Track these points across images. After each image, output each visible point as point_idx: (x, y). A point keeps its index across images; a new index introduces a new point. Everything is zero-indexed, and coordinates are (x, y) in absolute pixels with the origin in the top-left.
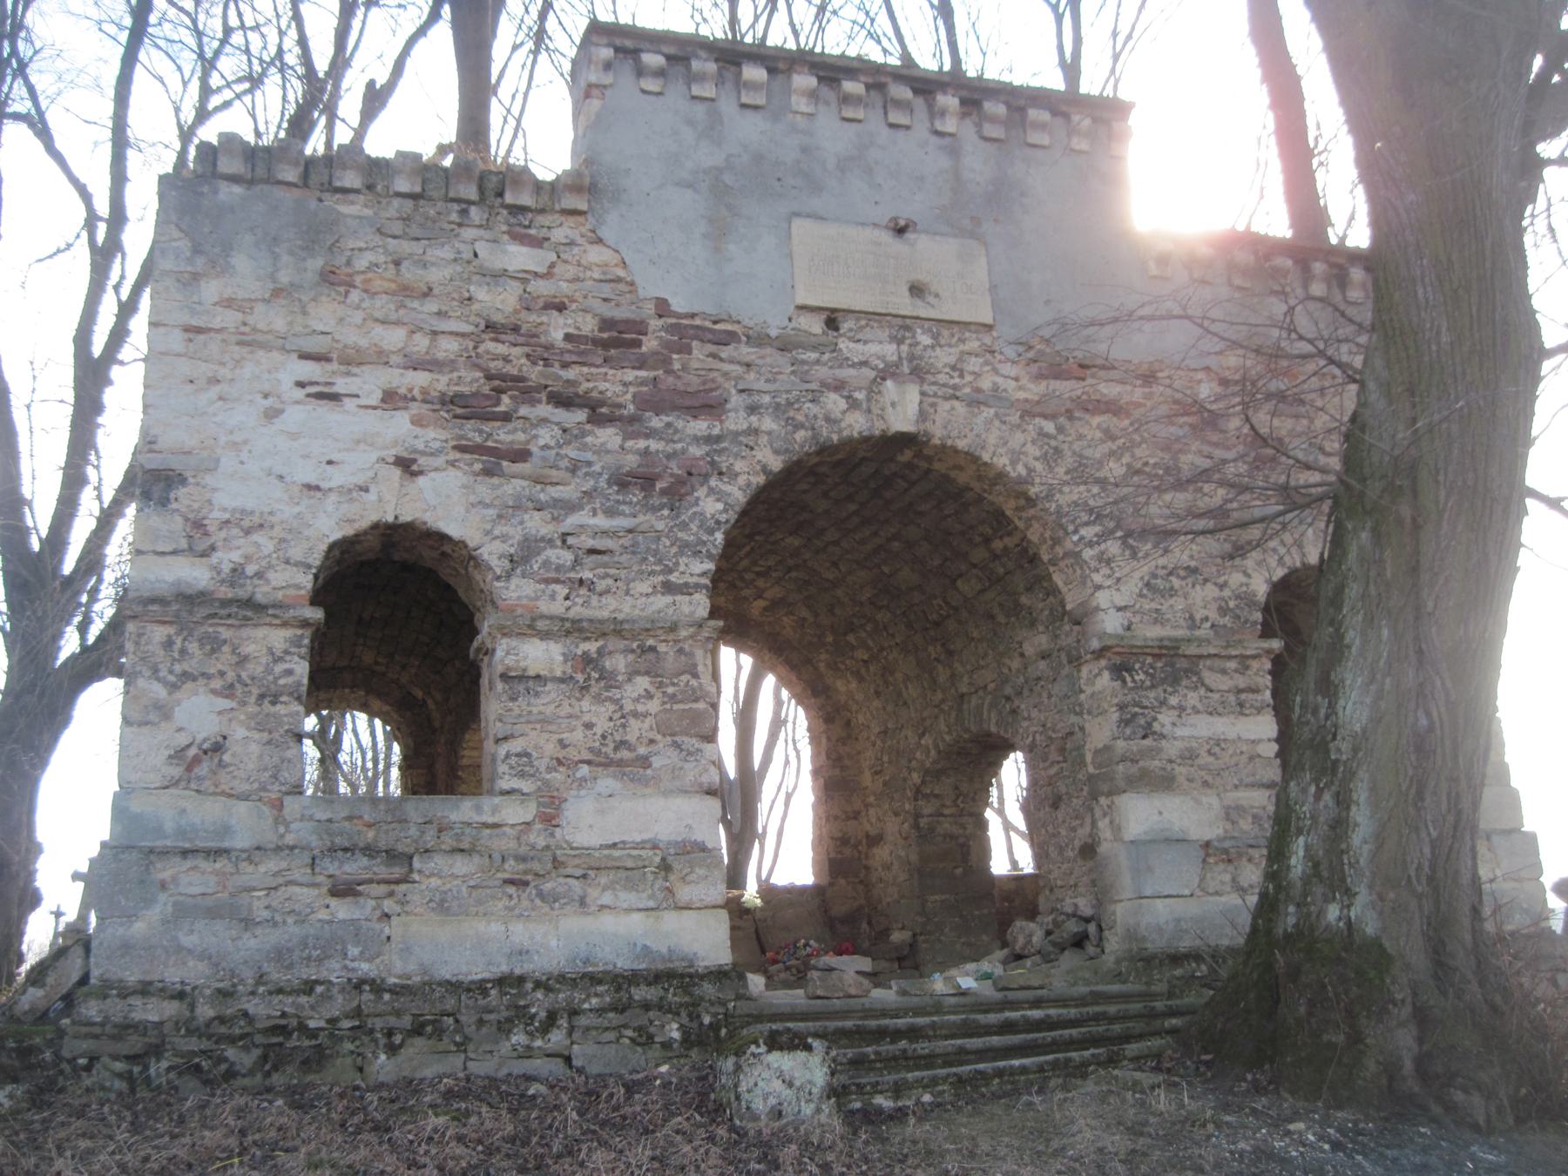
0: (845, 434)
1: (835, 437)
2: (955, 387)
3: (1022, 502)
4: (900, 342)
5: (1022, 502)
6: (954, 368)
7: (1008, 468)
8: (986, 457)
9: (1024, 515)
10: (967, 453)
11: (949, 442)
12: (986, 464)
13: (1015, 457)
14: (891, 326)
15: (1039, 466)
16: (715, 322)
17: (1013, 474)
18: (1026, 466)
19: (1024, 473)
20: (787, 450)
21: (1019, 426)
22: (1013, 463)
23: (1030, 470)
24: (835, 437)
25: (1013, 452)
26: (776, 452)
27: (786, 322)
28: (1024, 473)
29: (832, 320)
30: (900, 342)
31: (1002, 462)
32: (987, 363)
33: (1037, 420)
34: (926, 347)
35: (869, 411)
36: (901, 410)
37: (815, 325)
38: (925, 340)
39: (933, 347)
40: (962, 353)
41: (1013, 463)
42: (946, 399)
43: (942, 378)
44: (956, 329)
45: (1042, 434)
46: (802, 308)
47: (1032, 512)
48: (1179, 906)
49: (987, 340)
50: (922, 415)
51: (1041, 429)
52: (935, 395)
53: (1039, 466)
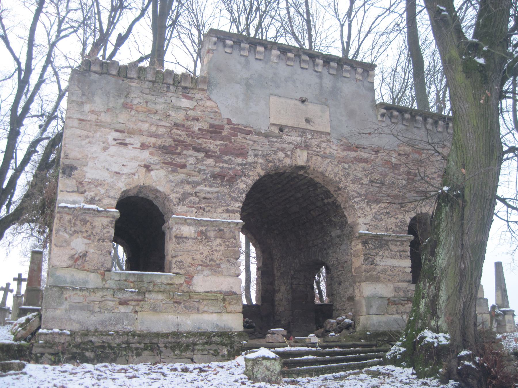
2: (318, 152)
3: (336, 189)
8: (327, 174)
9: (337, 193)
12: (326, 177)
19: (338, 180)
22: (335, 177)
28: (338, 180)
32: (328, 145)
34: (310, 139)
35: (292, 158)
36: (301, 158)
37: (276, 130)
41: (335, 177)
47: (339, 192)
49: (328, 138)
50: (308, 160)
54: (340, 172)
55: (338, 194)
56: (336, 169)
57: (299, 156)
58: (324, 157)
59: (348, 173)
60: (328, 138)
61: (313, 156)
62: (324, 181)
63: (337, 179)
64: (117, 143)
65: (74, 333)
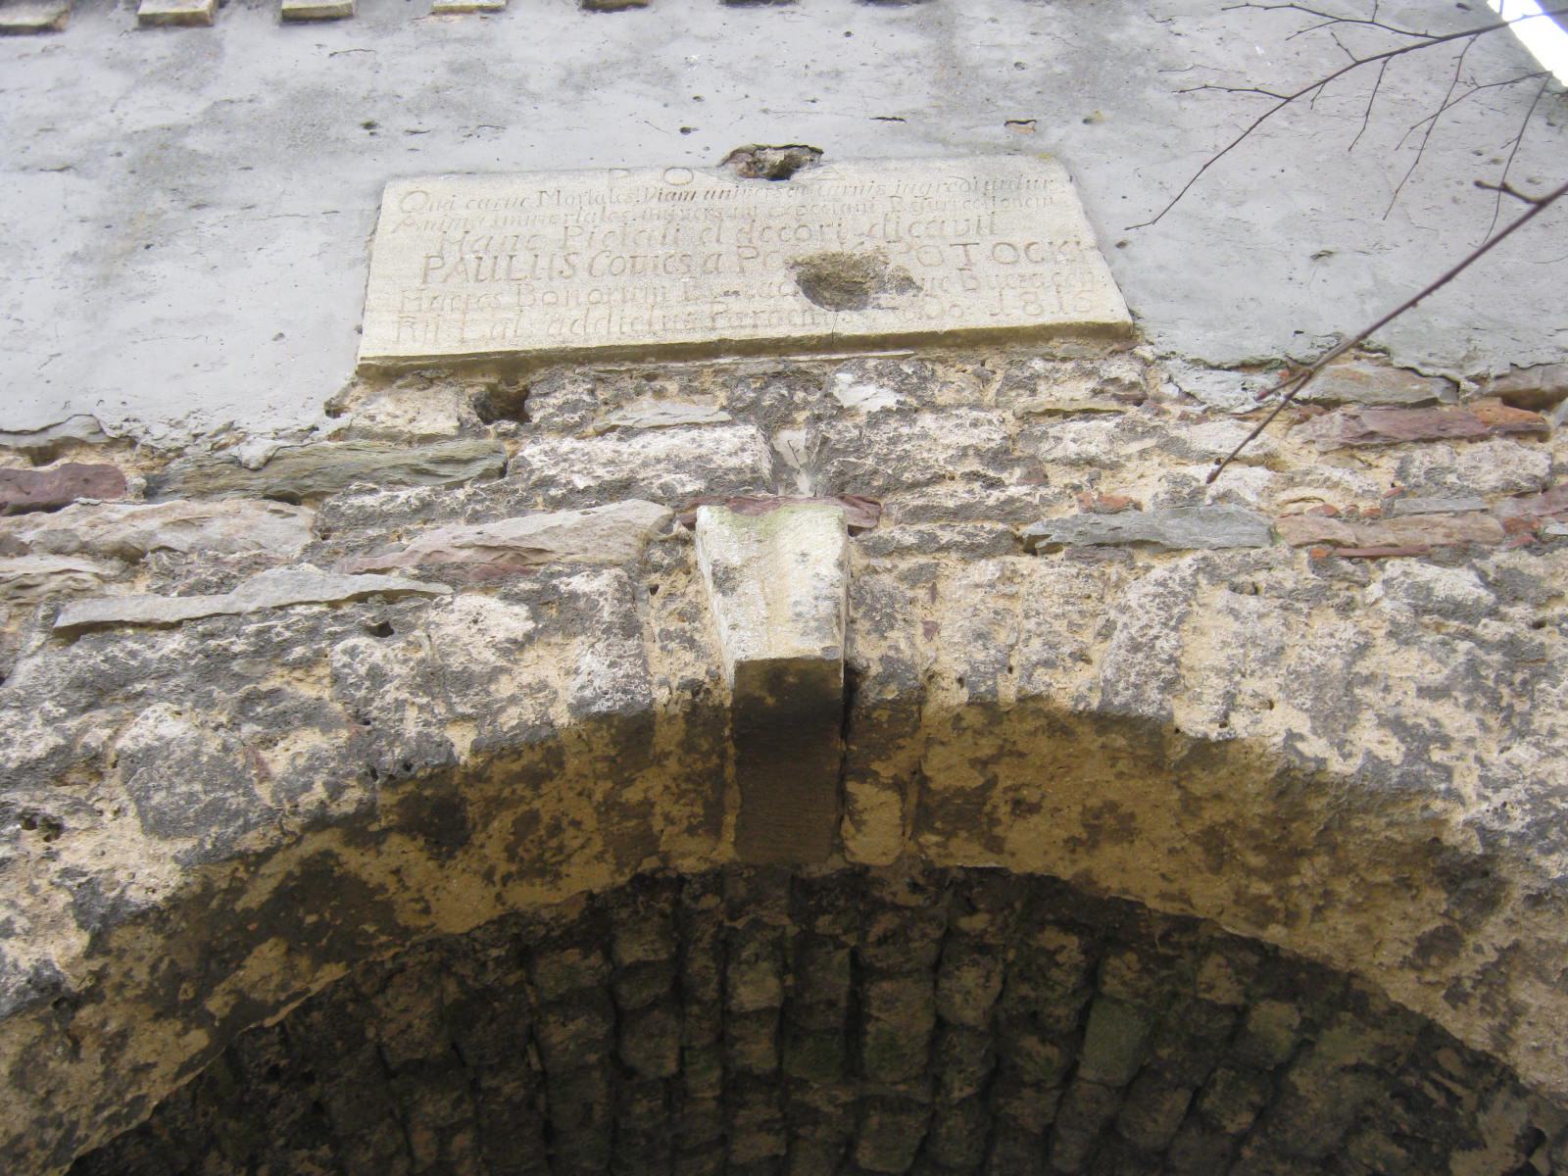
0: (509, 719)
1: (462, 740)
2: (1010, 511)
3: (1432, 907)
4: (773, 421)
5: (1432, 907)
6: (1000, 457)
7: (1315, 747)
8: (1195, 719)
9: (1466, 966)
10: (1103, 720)
11: (1008, 690)
12: (1205, 752)
13: (1336, 702)
14: (730, 380)
15: (1454, 717)
16: (42, 456)
17: (1337, 766)
18: (1396, 725)
19: (1392, 750)
20: (214, 811)
21: (1316, 597)
22: (1335, 719)
23: (1419, 739)
24: (462, 740)
25: (1320, 680)
26: (159, 826)
27: (315, 415)
28: (1392, 750)
29: (505, 389)
30: (773, 421)
31: (1277, 724)
32: (1131, 431)
33: (1394, 568)
34: (876, 420)
35: (630, 627)
36: (777, 593)
37: (438, 413)
38: (876, 397)
39: (905, 413)
40: (1026, 416)
41: (1335, 719)
42: (973, 551)
43: (952, 494)
44: (994, 360)
45: (1426, 605)
46: (385, 374)
47: (1493, 934)
48: (534, 378)
49: (1123, 370)
50: (858, 602)
51: (1426, 590)
52: (927, 544)
53: (1454, 717)
54: (1386, 657)
55: (1493, 978)
56: (1324, 638)
57: (725, 580)
58: (1115, 546)
59: (1511, 647)
60: (1123, 370)
61: (951, 561)
62: (1216, 847)
63: (1372, 740)
64: (166, 524)
65: (168, 744)
